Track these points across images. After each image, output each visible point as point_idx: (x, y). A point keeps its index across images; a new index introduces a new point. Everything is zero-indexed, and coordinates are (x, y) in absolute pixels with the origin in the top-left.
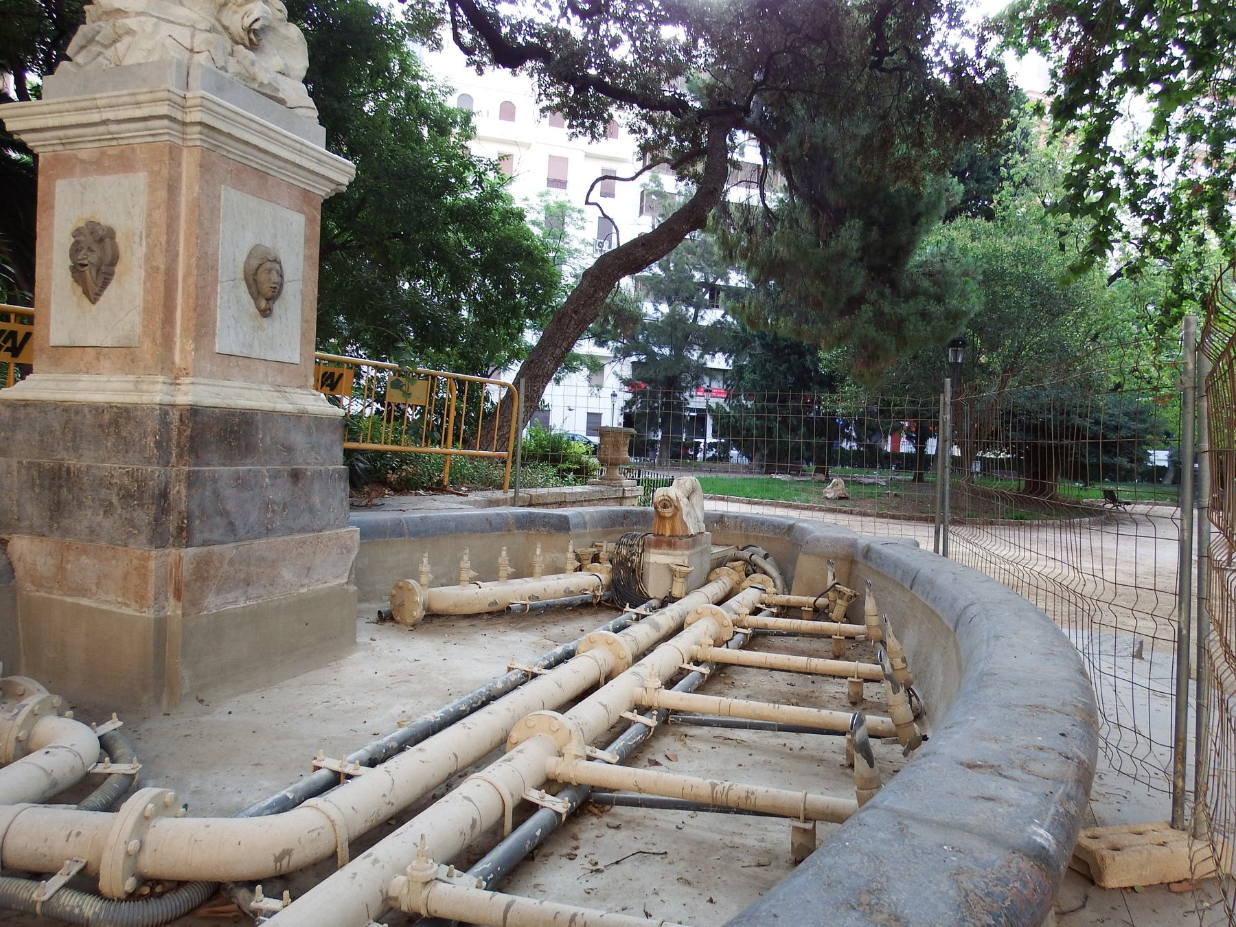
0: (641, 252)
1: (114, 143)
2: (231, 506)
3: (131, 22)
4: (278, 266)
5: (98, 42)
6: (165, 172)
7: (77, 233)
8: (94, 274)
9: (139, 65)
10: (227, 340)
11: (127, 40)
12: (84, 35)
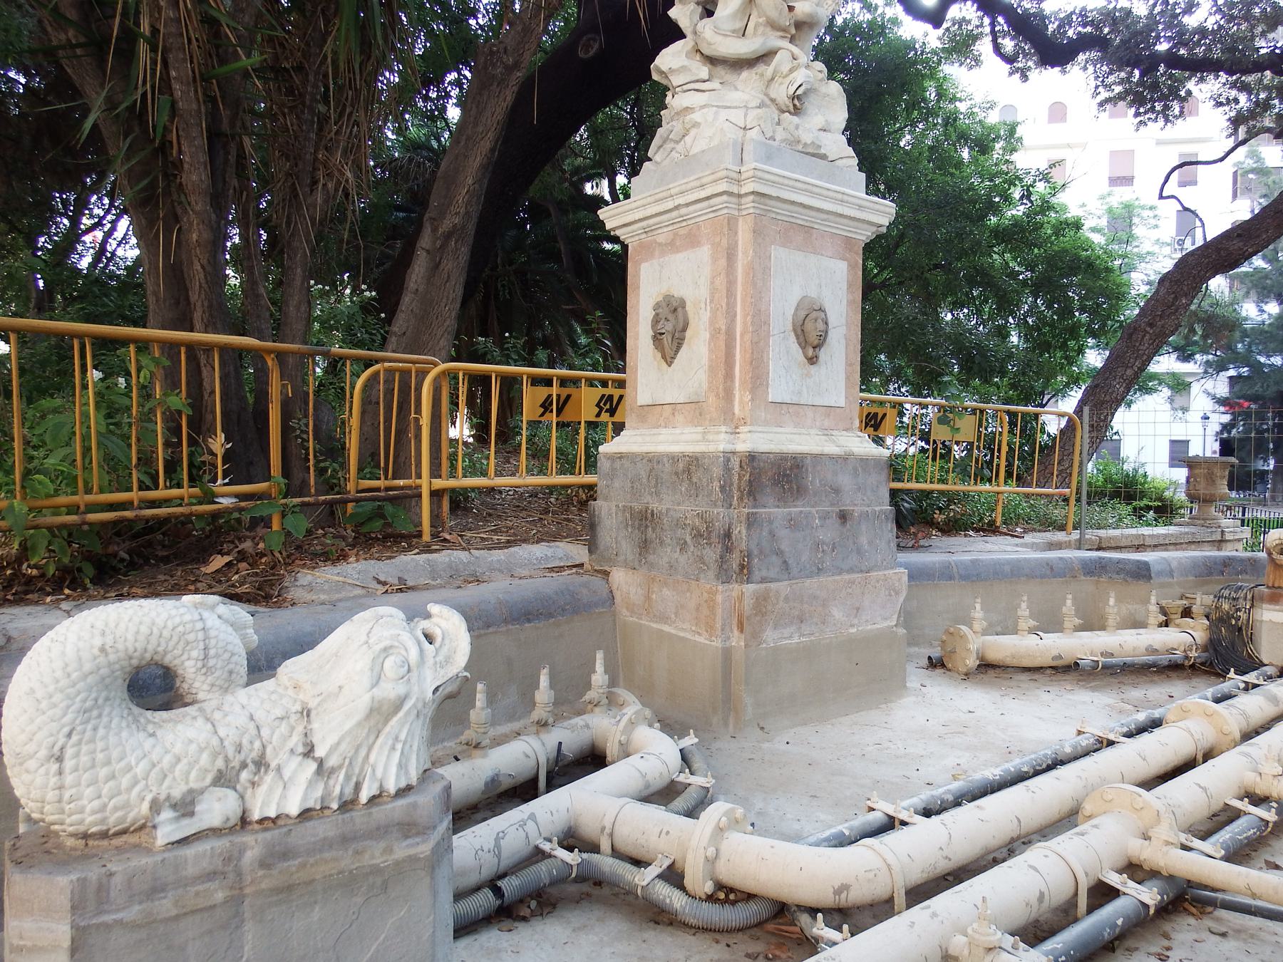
0: (1236, 244)
2: (784, 546)
6: (724, 242)
7: (657, 306)
10: (779, 390)
11: (693, 132)
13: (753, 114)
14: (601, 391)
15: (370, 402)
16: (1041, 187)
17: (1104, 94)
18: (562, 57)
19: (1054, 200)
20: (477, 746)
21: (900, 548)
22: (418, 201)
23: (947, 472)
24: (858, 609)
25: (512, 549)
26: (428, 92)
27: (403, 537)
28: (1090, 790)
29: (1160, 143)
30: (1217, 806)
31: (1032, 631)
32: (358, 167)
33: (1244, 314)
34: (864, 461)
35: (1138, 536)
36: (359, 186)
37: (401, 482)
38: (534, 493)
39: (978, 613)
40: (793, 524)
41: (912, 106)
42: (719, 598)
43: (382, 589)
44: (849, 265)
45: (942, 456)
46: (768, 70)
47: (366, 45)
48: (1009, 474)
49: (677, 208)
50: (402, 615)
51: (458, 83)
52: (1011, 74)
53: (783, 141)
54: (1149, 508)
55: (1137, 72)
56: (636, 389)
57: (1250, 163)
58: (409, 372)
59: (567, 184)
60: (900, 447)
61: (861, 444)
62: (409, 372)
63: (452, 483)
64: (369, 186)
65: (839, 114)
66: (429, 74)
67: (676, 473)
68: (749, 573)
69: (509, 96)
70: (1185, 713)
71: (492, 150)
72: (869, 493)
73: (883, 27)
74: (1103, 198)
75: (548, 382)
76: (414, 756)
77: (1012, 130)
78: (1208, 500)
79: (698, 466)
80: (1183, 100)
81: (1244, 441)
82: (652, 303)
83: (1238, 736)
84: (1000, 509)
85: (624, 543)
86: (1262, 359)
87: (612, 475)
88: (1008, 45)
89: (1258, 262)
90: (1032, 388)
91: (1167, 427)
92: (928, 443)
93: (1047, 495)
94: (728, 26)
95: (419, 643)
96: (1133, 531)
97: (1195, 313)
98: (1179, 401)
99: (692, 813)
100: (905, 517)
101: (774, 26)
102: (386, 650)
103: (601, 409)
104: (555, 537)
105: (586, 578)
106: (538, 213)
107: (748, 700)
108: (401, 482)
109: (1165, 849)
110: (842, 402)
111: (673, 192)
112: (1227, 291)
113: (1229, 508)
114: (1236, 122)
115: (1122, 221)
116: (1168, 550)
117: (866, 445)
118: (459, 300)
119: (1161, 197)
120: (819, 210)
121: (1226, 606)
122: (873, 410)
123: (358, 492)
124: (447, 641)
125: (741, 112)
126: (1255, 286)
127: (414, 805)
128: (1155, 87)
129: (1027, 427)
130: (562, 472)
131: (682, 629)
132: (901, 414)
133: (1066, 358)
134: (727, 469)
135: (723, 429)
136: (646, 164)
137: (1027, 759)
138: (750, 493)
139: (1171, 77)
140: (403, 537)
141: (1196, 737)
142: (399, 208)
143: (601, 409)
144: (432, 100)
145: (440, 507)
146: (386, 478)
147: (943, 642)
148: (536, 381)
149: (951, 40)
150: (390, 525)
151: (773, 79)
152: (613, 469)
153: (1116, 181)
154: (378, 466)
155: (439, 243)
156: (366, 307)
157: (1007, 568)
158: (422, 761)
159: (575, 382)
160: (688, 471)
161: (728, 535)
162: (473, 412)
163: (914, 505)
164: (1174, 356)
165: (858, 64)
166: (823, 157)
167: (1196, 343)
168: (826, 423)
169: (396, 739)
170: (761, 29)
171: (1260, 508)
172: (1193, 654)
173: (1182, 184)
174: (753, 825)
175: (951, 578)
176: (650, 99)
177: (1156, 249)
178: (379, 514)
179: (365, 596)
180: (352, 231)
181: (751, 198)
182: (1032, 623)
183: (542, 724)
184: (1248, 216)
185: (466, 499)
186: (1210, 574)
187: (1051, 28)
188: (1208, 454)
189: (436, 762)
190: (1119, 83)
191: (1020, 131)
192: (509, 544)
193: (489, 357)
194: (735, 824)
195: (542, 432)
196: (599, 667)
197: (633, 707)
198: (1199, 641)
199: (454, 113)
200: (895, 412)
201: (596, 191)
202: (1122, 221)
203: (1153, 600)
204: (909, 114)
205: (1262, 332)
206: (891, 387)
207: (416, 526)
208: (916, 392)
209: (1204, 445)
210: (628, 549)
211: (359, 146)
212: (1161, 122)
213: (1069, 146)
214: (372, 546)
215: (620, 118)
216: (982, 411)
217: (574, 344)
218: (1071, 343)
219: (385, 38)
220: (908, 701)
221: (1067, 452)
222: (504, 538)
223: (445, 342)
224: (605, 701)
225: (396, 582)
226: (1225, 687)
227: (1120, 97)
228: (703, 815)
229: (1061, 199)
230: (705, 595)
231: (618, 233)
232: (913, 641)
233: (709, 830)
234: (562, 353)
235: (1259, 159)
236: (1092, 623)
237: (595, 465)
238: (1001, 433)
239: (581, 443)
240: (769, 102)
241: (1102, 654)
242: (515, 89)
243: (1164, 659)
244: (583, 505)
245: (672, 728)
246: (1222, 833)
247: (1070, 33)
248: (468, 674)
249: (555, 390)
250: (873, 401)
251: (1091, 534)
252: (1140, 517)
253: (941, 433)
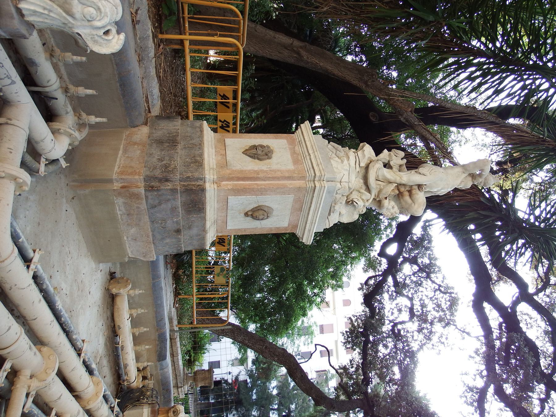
0: (299, 375)
2: (163, 206)
3: (346, 162)
7: (268, 147)
10: (233, 200)
11: (339, 161)
13: (346, 185)
14: (231, 122)
15: (225, 12)
16: (319, 300)
17: (354, 319)
18: (370, 106)
19: (314, 305)
20: (52, 56)
21: (166, 257)
22: (314, 41)
23: (201, 274)
24: (136, 240)
25: (156, 79)
26: (358, 47)
27: (160, 24)
28: (55, 349)
29: (336, 342)
30: (51, 405)
31: (131, 315)
32: (327, 13)
33: (272, 382)
34: (203, 239)
35: (177, 354)
36: (320, 13)
37: (187, 25)
38: (184, 90)
39: (137, 292)
40: (174, 209)
41: (349, 248)
42: (137, 177)
43: (133, 11)
44: (286, 227)
45: (207, 271)
46: (363, 191)
47: (377, 20)
48: (201, 299)
49: (309, 155)
50: (118, 19)
51: (361, 60)
52: (361, 284)
53: (336, 198)
54: (190, 356)
55: (362, 330)
56: (232, 138)
57: (330, 375)
58: (239, 32)
59: (320, 108)
60: (211, 253)
61: (211, 237)
62: (239, 32)
63: (187, 50)
64: (321, 18)
65: (346, 220)
66: (366, 49)
67: (194, 157)
68: (150, 191)
69: (355, 82)
70: (97, 384)
71: (334, 75)
72: (190, 241)
73: (379, 234)
74: (315, 323)
75: (235, 98)
76: (41, 20)
77: (340, 286)
78: (195, 379)
79: (198, 166)
80: (352, 348)
81: (221, 389)
82: (270, 144)
83: (88, 408)
84: (186, 297)
85: (161, 132)
86: (254, 391)
87: (193, 127)
88: (372, 282)
89: (292, 384)
90: (239, 305)
91: (225, 358)
92: (213, 265)
93: (193, 315)
94: (380, 173)
95: (104, 27)
96: (179, 351)
97: (271, 363)
98: (236, 362)
99: (23, 165)
100: (180, 257)
101: (380, 192)
102: (98, 9)
103: (223, 122)
104: (163, 99)
105: (144, 114)
106: (308, 95)
107: (87, 191)
108: (187, 25)
109: (26, 386)
110: (229, 228)
111: (316, 153)
112: (281, 374)
113: (192, 388)
114: (345, 368)
115: (307, 332)
116: (172, 366)
117: (211, 239)
118: (271, 57)
119: (316, 345)
120: (308, 214)
121: (148, 393)
122: (226, 241)
123: (182, 3)
124: (105, 42)
125: (347, 180)
126: (283, 384)
127: (12, 17)
128: (357, 337)
129: (222, 305)
130: (194, 103)
131: (120, 160)
132: (225, 253)
133: (252, 317)
134: (198, 179)
135: (215, 177)
136: (327, 141)
137: (68, 319)
138: (187, 190)
139: (361, 343)
140: (160, 24)
141: (86, 391)
142: (311, 32)
143: (223, 122)
144: (355, 49)
145: (176, 44)
146: (189, 18)
147: (123, 278)
148: (235, 92)
149: (373, 260)
150: (166, 18)
152: (196, 127)
153: (322, 327)
154: (195, 14)
155: (295, 49)
156: (268, 14)
157: (159, 302)
158: (38, 24)
159: (235, 111)
160: (196, 161)
161: (167, 180)
162: (220, 62)
163: (185, 261)
164: (254, 358)
165: (365, 225)
166: (329, 214)
167: (260, 365)
168: (219, 222)
169: (50, 11)
171: (193, 400)
172: (126, 383)
173: (321, 352)
174: (20, 195)
175: (153, 279)
176: (353, 143)
177: (296, 345)
178: (171, 13)
179: (129, 3)
180: (302, 9)
181: (313, 186)
182: (135, 315)
183: (66, 90)
184: (310, 378)
185: (180, 57)
186: (163, 385)
187: (378, 297)
188: (214, 376)
189: (41, 32)
190: (358, 324)
191: (340, 289)
192: (159, 77)
193: (246, 71)
194: (19, 186)
195: (213, 95)
196: (98, 120)
197: (79, 136)
198: (132, 385)
199: (349, 58)
200: (226, 250)
201: (317, 120)
202: (307, 332)
203: (149, 364)
204: (346, 247)
205: (265, 390)
206: (237, 248)
207: (166, 31)
208: (235, 259)
209: (218, 374)
210: (158, 134)
211: (336, 14)
212: (344, 341)
213: (334, 308)
214: (155, 8)
215: (345, 130)
216: (228, 286)
217: (252, 111)
218: (257, 318)
219: (380, 29)
220: (93, 265)
221: (212, 322)
222: (161, 75)
223: (252, 50)
224: (81, 122)
225: (138, 19)
226: (111, 399)
227: (353, 325)
228: (22, 171)
229: (315, 308)
230: (138, 171)
231: (299, 129)
232: (122, 265)
233: (14, 173)
234: (248, 105)
235: (331, 379)
236: (137, 340)
237: (198, 119)
238: (219, 294)
239: (207, 112)
240: (351, 191)
241: (122, 346)
242: (358, 85)
243: (122, 371)
244: (179, 114)
245: (69, 155)
246: (37, 410)
247: (376, 304)
248: (89, 52)
249: (231, 101)
250: (230, 241)
251: (177, 335)
252: (186, 353)
253: (217, 269)
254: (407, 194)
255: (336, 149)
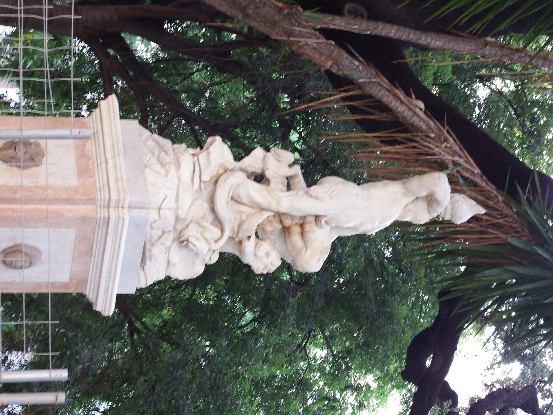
1: (96, 165)
4: (28, 265)
5: (160, 153)
6: (78, 196)
8: (11, 155)
9: (145, 179)
11: (163, 171)
12: (164, 145)
53: (151, 235)
151: (201, 226)
166: (143, 261)
170: (238, 216)
181: (107, 215)
254: (296, 230)
255: (162, 148)
